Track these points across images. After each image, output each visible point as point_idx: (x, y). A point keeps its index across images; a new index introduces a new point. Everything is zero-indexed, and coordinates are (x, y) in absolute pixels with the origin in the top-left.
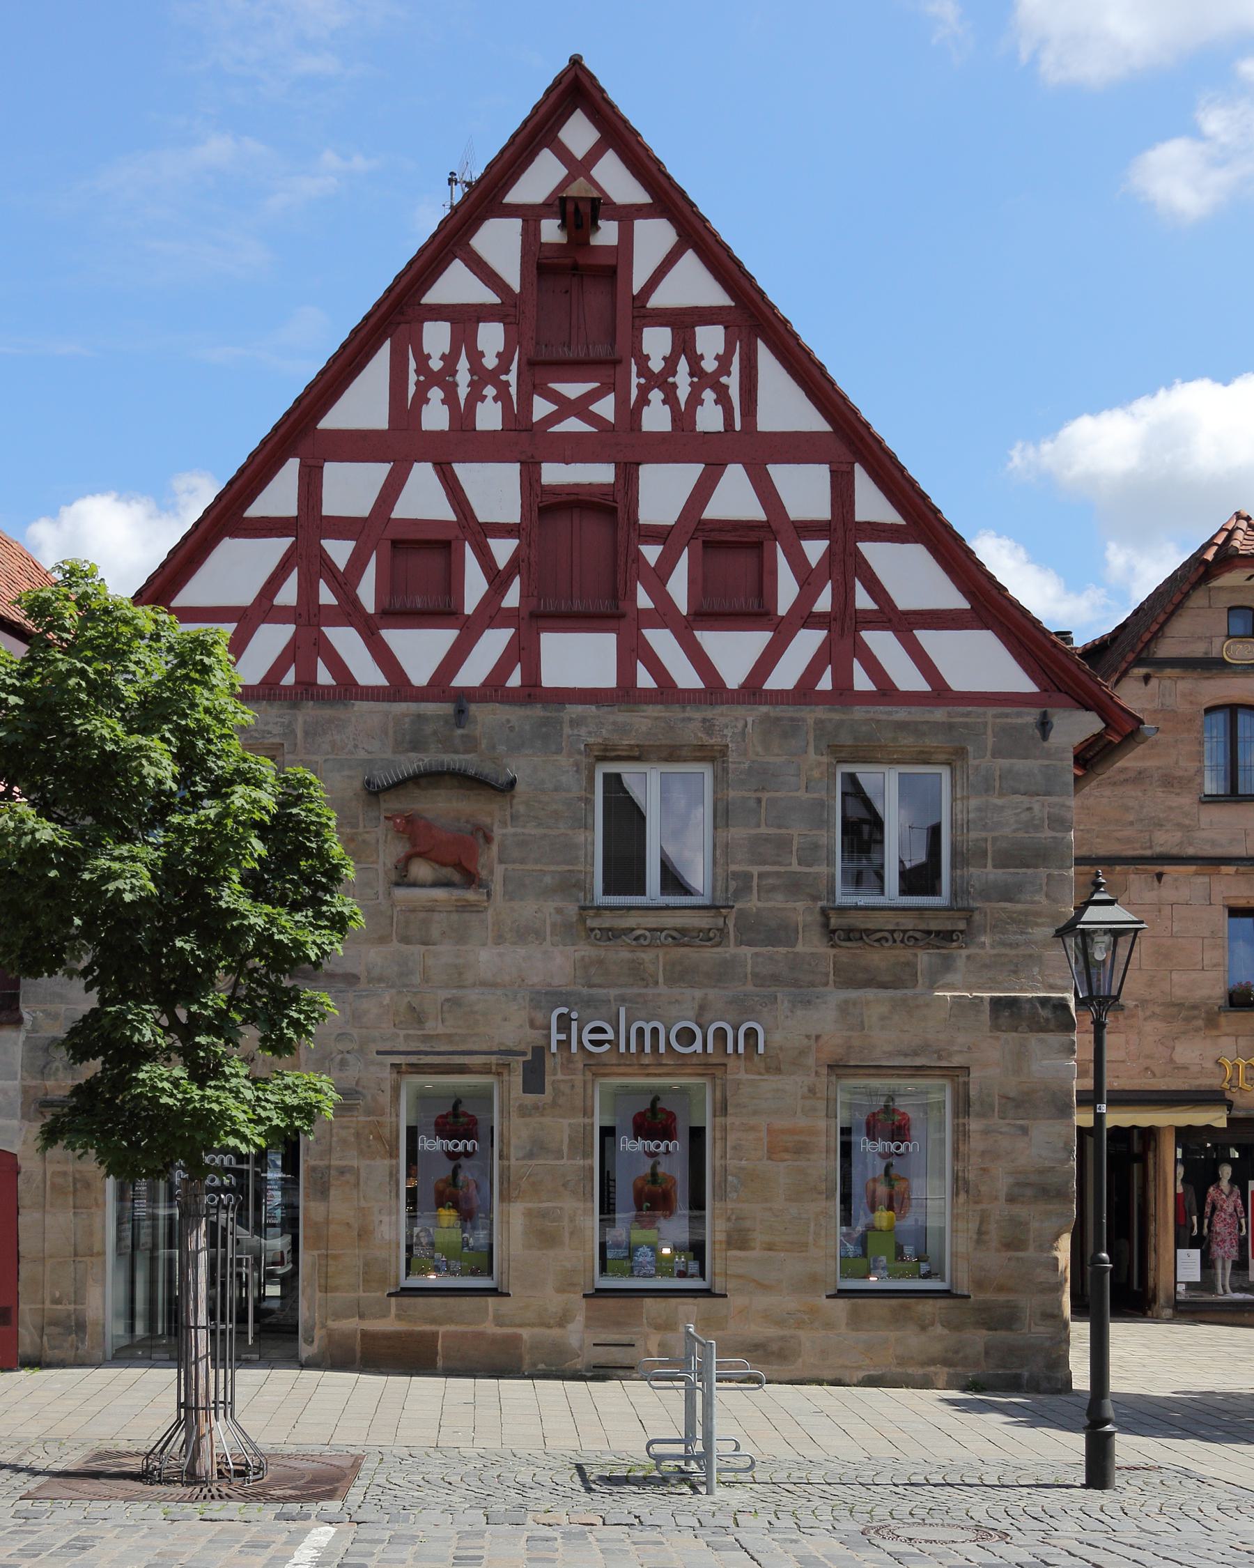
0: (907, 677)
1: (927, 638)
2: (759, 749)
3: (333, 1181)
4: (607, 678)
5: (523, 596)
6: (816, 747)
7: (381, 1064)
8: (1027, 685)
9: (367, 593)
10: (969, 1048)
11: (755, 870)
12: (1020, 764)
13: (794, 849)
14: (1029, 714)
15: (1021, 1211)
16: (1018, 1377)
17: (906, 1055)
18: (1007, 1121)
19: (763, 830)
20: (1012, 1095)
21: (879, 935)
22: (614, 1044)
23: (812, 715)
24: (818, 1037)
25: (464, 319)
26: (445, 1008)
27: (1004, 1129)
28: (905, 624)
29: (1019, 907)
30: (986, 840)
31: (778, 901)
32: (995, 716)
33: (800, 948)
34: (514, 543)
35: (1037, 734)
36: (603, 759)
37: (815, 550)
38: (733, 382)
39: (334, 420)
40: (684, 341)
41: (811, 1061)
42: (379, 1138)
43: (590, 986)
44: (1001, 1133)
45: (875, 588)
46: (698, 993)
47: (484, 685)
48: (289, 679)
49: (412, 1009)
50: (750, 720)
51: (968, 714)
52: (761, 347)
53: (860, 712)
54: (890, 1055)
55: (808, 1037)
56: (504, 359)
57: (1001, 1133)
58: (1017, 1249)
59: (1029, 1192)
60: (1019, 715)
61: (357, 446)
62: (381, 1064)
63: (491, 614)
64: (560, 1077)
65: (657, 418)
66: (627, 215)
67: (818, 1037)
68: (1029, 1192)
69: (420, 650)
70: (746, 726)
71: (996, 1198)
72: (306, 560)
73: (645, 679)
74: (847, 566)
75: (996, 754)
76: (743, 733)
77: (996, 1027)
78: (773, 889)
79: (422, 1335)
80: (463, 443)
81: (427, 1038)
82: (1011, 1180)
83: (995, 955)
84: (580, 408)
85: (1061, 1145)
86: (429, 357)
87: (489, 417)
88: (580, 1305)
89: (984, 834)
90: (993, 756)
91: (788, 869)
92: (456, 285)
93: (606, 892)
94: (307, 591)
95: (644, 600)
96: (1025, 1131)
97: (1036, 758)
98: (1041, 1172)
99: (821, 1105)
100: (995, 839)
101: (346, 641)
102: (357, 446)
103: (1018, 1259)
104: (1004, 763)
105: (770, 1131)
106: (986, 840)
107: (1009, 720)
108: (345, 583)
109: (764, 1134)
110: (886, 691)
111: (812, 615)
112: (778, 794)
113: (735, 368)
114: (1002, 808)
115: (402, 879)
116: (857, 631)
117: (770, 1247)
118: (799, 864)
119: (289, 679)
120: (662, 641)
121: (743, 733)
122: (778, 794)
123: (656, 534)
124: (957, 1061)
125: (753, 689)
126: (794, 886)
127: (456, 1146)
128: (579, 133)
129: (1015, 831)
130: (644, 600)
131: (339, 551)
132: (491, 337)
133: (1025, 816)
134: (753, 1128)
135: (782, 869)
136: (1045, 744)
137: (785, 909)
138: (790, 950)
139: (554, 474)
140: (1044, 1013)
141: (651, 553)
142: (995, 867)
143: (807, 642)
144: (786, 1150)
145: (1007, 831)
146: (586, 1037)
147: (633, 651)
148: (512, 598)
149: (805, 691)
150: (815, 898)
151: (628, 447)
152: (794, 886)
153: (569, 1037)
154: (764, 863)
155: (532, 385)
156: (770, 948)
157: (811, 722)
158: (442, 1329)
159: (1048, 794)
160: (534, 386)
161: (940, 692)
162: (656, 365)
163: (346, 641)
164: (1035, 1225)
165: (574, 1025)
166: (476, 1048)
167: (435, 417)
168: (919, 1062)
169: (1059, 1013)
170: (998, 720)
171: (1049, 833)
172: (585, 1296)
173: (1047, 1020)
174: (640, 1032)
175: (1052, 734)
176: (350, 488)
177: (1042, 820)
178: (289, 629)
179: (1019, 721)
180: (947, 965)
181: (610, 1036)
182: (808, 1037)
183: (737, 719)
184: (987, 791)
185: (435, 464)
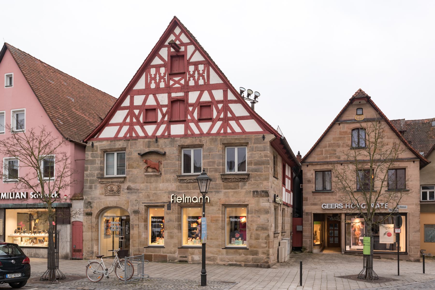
15: (259, 232)
22: (182, 201)
29: (259, 173)
81: (151, 200)
92: (157, 61)
96: (259, 217)
98: (262, 225)
133: (260, 155)
158: (153, 254)
159: (264, 151)
164: (261, 235)
171: (265, 159)
174: (187, 198)
180: (245, 185)
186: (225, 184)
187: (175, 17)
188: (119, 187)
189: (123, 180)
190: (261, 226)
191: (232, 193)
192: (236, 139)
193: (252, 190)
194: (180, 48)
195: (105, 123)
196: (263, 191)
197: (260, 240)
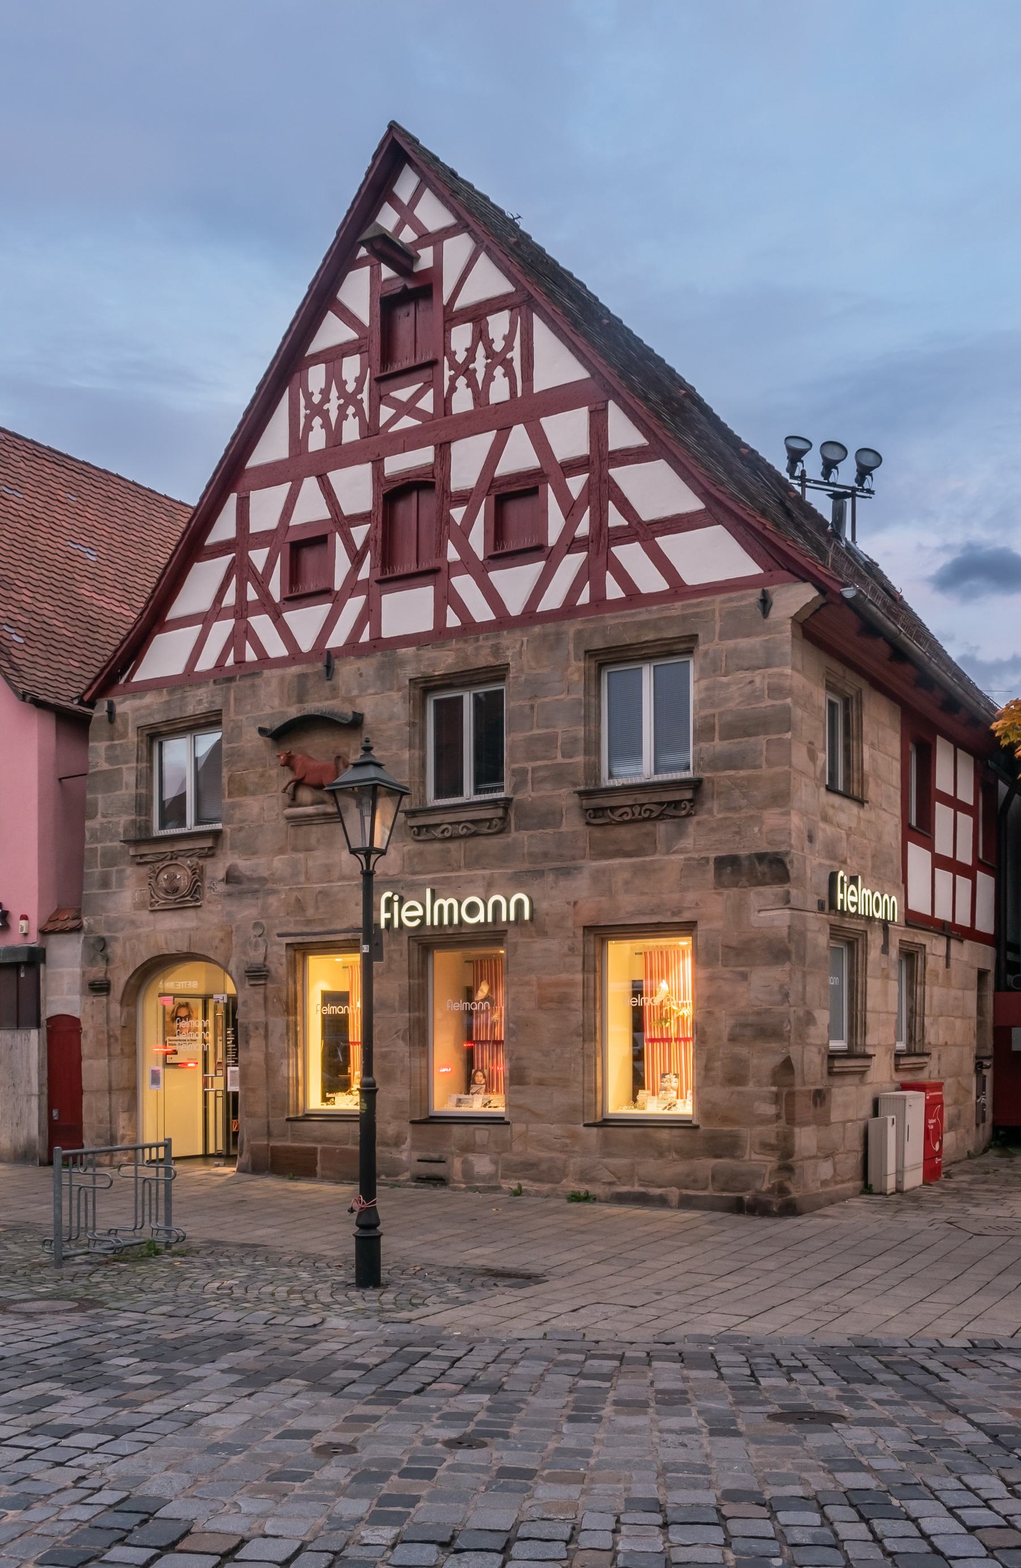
0: (650, 580)
1: (665, 542)
2: (533, 664)
3: (252, 1034)
4: (426, 624)
5: (372, 568)
6: (576, 654)
7: (280, 944)
8: (755, 569)
9: (275, 588)
10: (697, 904)
11: (530, 765)
12: (743, 643)
13: (559, 744)
14: (751, 595)
15: (743, 1051)
16: (740, 1200)
17: (644, 914)
18: (729, 969)
19: (536, 731)
20: (734, 944)
21: (622, 810)
22: (423, 918)
23: (571, 627)
24: (575, 903)
25: (333, 357)
26: (319, 898)
27: (727, 976)
28: (645, 532)
29: (742, 773)
30: (714, 715)
31: (547, 790)
32: (724, 602)
33: (564, 828)
34: (366, 527)
35: (759, 611)
36: (426, 691)
37: (576, 484)
38: (515, 355)
39: (255, 460)
40: (481, 331)
41: (569, 923)
42: (280, 1000)
43: (414, 873)
44: (724, 979)
45: (625, 507)
46: (487, 872)
47: (346, 644)
48: (584, 598)
49: (298, 900)
50: (525, 639)
51: (698, 605)
52: (536, 318)
53: (611, 619)
54: (632, 914)
55: (568, 903)
56: (360, 381)
57: (724, 979)
58: (739, 1084)
59: (748, 1032)
60: (743, 598)
61: (271, 475)
62: (280, 944)
63: (353, 587)
64: (392, 947)
65: (462, 402)
66: (435, 239)
67: (575, 903)
68: (748, 1032)
69: (306, 623)
70: (522, 645)
71: (720, 1038)
72: (241, 571)
73: (453, 620)
74: (603, 492)
75: (724, 636)
76: (520, 652)
77: (720, 883)
78: (544, 780)
79: (309, 1149)
80: (338, 454)
81: (309, 922)
82: (731, 1022)
83: (721, 819)
84: (408, 408)
85: (776, 988)
86: (312, 394)
87: (351, 432)
88: (408, 1131)
89: (711, 711)
90: (720, 639)
91: (555, 762)
92: (333, 332)
93: (438, 795)
94: (241, 591)
95: (452, 554)
96: (744, 977)
97: (758, 634)
98: (758, 1014)
99: (578, 961)
100: (721, 714)
101: (262, 624)
102: (271, 475)
103: (740, 1093)
104: (730, 643)
105: (540, 986)
106: (714, 715)
107: (734, 604)
108: (262, 582)
109: (534, 989)
110: (634, 597)
111: (574, 540)
112: (546, 700)
113: (517, 343)
114: (727, 685)
115: (294, 801)
116: (609, 548)
117: (541, 1083)
118: (563, 756)
119: (584, 598)
120: (464, 585)
121: (520, 652)
122: (546, 700)
123: (463, 498)
124: (686, 916)
125: (530, 615)
126: (559, 775)
127: (340, 1010)
128: (406, 186)
129: (738, 704)
130: (452, 554)
131: (258, 557)
132: (351, 367)
133: (748, 689)
134: (528, 983)
135: (549, 762)
136: (767, 621)
137: (552, 796)
138: (556, 830)
139: (396, 464)
140: (761, 868)
141: (458, 514)
142: (722, 739)
143: (572, 563)
144: (552, 1000)
145: (731, 705)
146: (405, 914)
147: (447, 598)
148: (364, 573)
149: (569, 609)
150: (575, 784)
151: (443, 430)
152: (559, 775)
153: (392, 915)
154: (537, 759)
155: (378, 399)
156: (541, 831)
157: (571, 633)
159: (768, 666)
160: (381, 398)
161: (678, 589)
162: (461, 357)
163: (262, 624)
164: (755, 1061)
165: (396, 905)
166: (339, 927)
167: (317, 440)
168: (655, 919)
169: (774, 866)
170: (726, 605)
172: (413, 1122)
173: (764, 874)
174: (441, 907)
175: (772, 610)
176: (266, 508)
177: (763, 690)
178: (231, 622)
179: (743, 603)
180: (681, 833)
181: (420, 913)
182: (568, 903)
183: (516, 641)
184: (714, 671)
185: (317, 477)
186: (597, 833)
187: (393, 127)
188: (198, 874)
189: (208, 843)
190: (751, 1019)
191: (626, 875)
192: (644, 625)
193: (713, 855)
194: (414, 259)
195: (155, 619)
196: (761, 857)
197: (750, 1087)
